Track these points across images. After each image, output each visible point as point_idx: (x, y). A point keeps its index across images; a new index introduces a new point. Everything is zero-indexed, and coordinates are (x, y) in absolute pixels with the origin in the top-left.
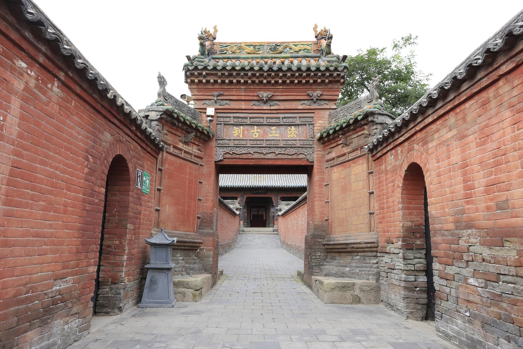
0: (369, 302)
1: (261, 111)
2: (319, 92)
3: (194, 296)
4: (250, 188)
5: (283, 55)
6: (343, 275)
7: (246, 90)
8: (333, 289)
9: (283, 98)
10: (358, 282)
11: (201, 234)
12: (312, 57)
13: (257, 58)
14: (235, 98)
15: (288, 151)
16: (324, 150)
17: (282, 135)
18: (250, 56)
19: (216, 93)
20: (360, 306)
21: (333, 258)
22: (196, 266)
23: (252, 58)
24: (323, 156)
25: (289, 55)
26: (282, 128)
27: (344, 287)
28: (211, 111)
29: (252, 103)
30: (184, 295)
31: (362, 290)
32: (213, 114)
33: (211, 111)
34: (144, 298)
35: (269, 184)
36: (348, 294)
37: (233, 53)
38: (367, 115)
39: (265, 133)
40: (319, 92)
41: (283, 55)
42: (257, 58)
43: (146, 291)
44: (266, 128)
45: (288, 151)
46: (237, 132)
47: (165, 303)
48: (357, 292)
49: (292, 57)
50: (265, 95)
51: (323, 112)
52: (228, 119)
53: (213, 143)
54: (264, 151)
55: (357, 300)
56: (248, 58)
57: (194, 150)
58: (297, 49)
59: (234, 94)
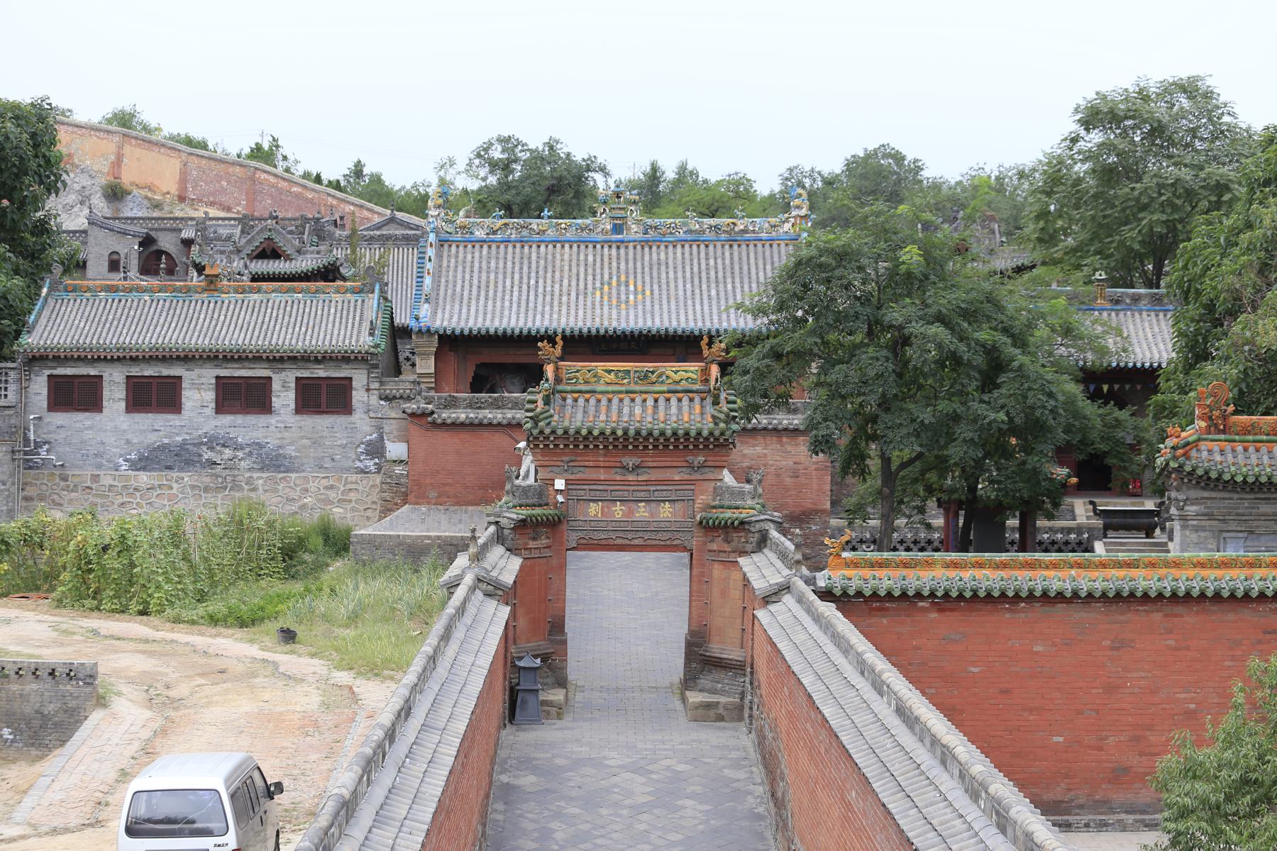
0: (732, 720)
1: (625, 483)
2: (701, 459)
3: (559, 714)
4: (589, 336)
5: (657, 388)
6: (713, 691)
7: (605, 455)
8: (697, 708)
9: (655, 464)
10: (723, 700)
11: (552, 641)
12: (696, 392)
13: (620, 392)
14: (591, 464)
15: (659, 536)
16: (706, 536)
17: (652, 515)
18: (610, 388)
19: (567, 459)
20: (723, 724)
21: (710, 671)
22: (549, 680)
23: (613, 392)
24: (705, 543)
25: (665, 388)
26: (653, 505)
27: (708, 706)
28: (560, 484)
29: (614, 470)
30: (548, 713)
31: (725, 708)
32: (563, 488)
33: (560, 484)
34: (517, 716)
35: (658, 324)
36: (712, 713)
37: (586, 382)
38: (742, 523)
39: (631, 512)
40: (701, 459)
41: (657, 388)
42: (620, 392)
43: (518, 710)
44: (631, 504)
45: (659, 536)
46: (594, 510)
47: (536, 720)
48: (721, 711)
49: (669, 392)
50: (630, 461)
51: (706, 483)
52: (582, 493)
53: (564, 527)
54: (630, 536)
55: (721, 718)
56: (608, 392)
57: (544, 542)
58: (677, 377)
59: (589, 460)
